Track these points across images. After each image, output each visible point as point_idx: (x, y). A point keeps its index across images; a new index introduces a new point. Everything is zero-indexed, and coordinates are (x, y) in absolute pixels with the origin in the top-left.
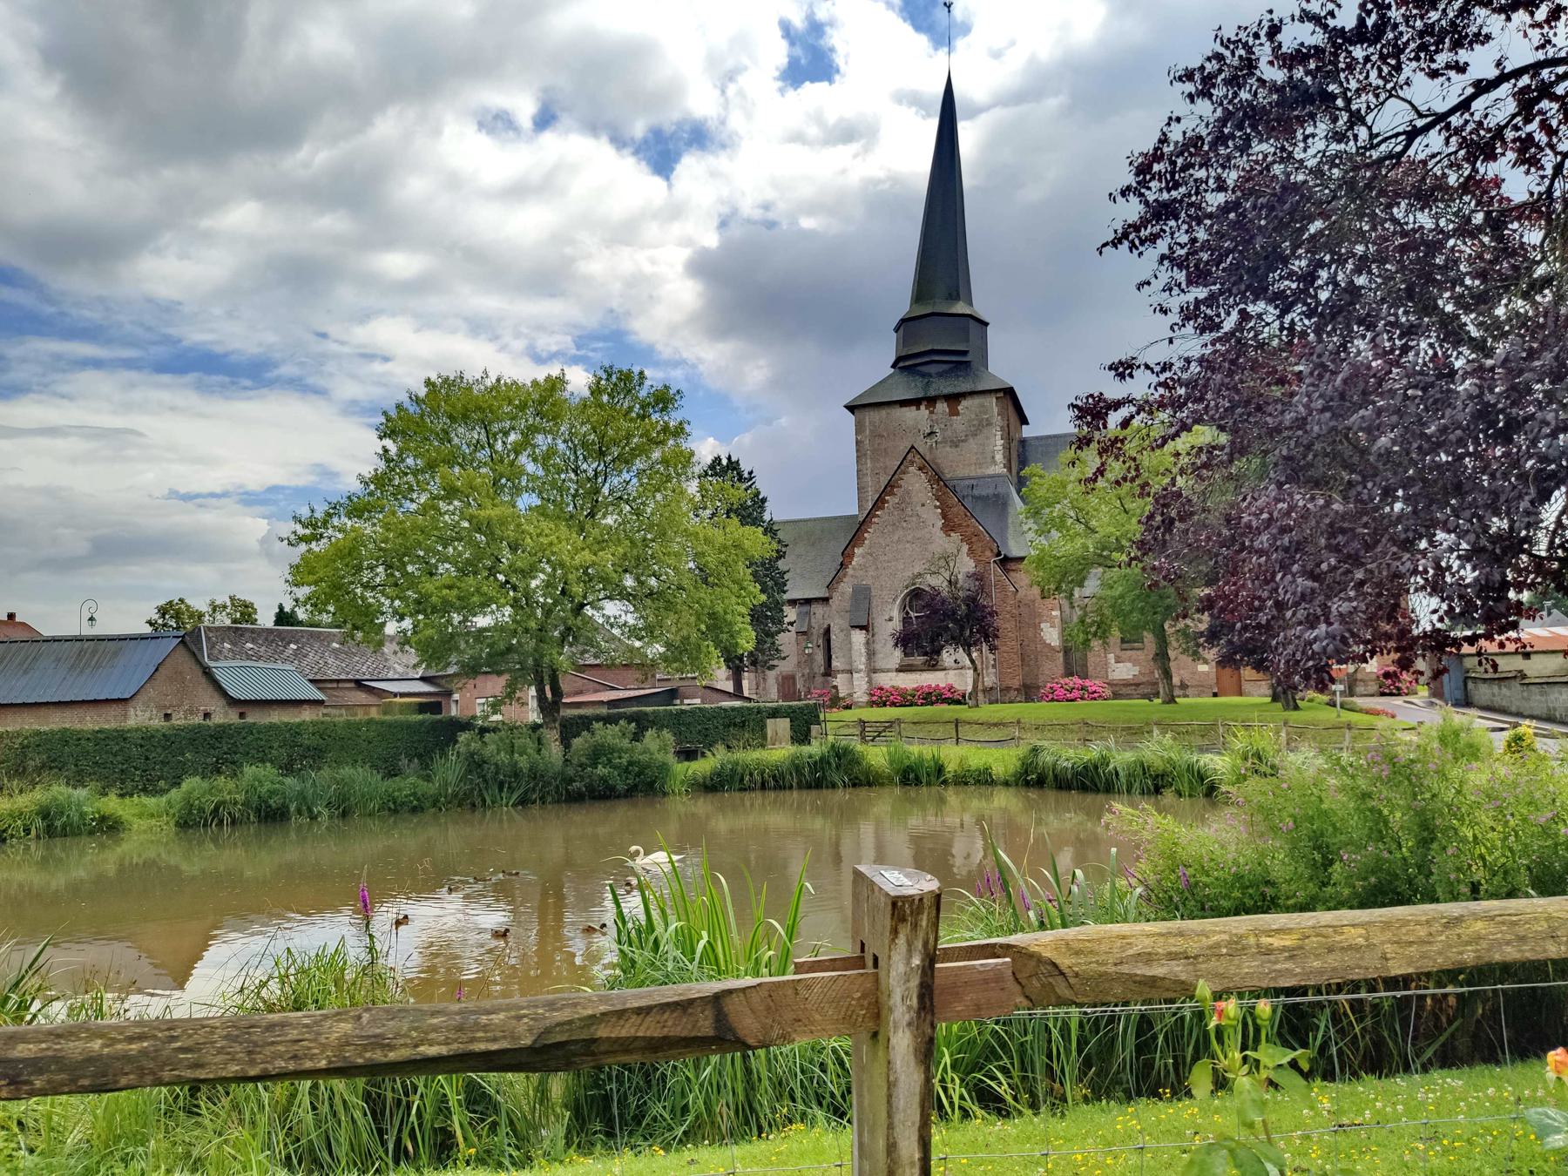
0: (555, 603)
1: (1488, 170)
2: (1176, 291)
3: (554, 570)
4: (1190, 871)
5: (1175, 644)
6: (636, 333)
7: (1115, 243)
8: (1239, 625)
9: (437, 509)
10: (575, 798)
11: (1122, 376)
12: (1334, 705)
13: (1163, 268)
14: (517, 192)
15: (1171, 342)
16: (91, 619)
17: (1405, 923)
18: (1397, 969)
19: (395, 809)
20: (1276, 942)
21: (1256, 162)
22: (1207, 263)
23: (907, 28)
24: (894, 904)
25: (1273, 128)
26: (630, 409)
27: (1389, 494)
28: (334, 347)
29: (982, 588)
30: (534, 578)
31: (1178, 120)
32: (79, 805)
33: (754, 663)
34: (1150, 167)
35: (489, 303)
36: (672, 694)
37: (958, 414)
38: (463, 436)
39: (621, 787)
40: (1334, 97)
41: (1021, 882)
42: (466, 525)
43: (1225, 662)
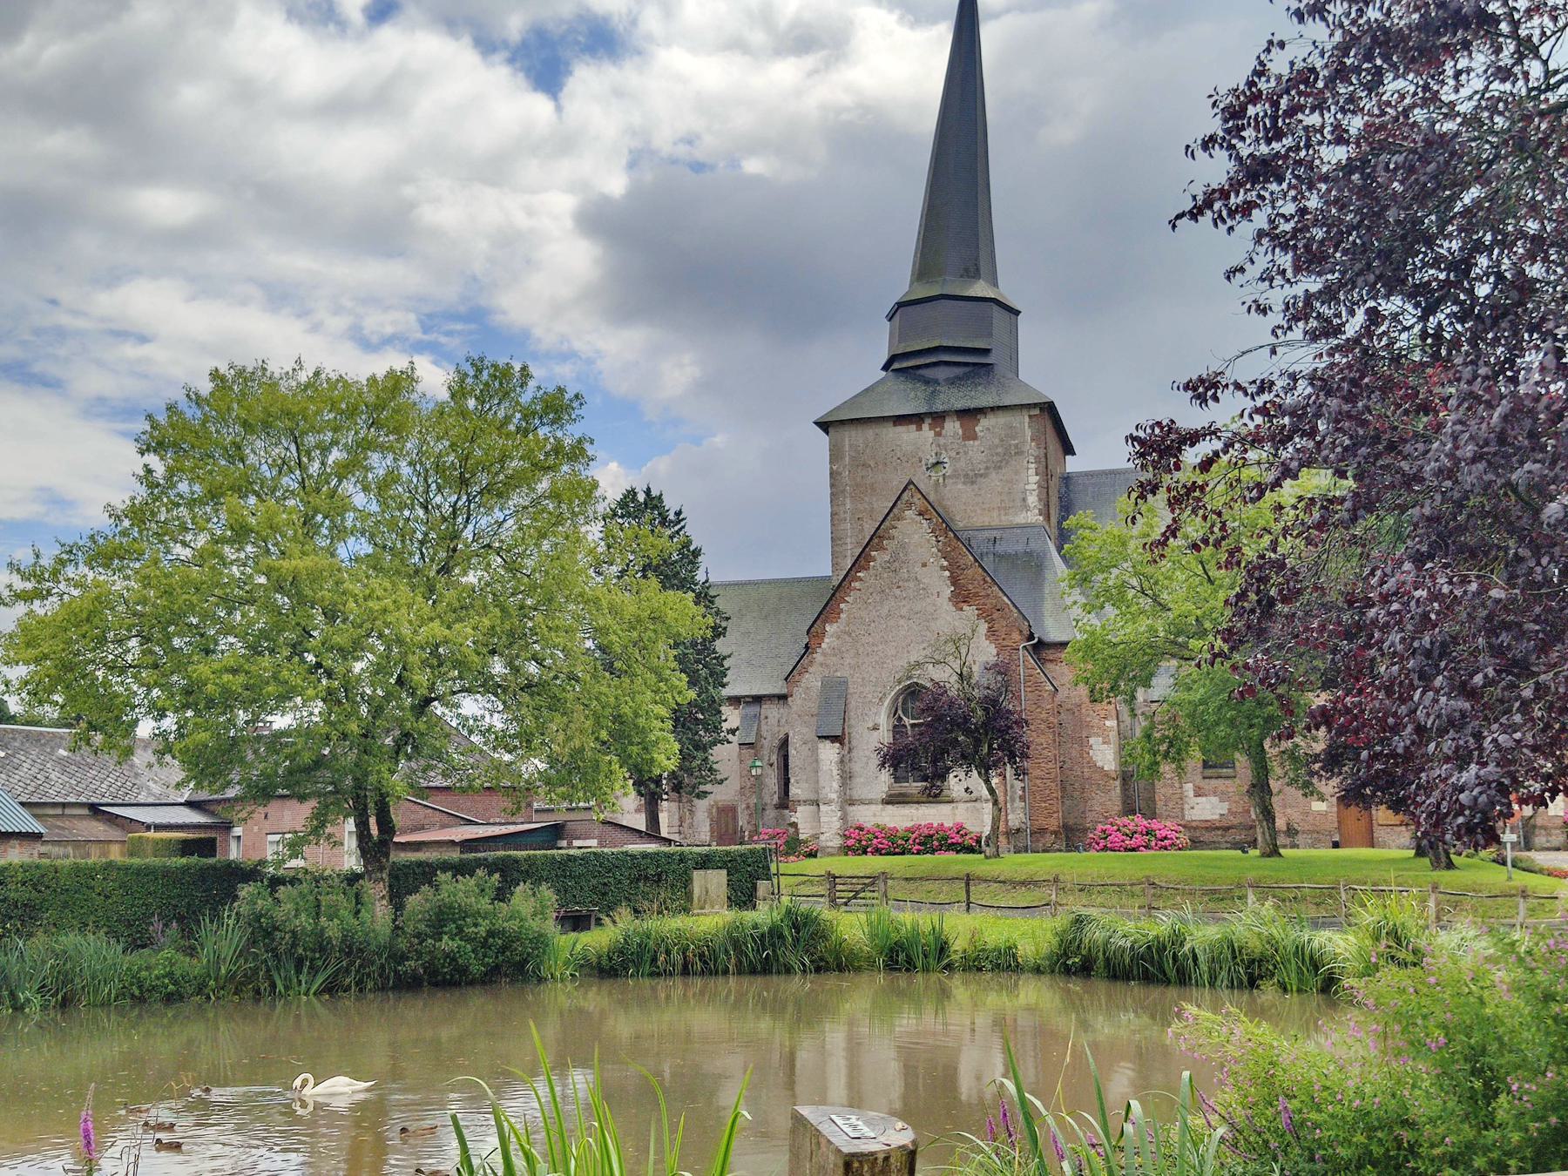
0: (389, 696)
2: (1278, 280)
3: (389, 648)
4: (1295, 1104)
5: (1279, 771)
6: (504, 313)
7: (1195, 214)
8: (1364, 754)
9: (222, 558)
10: (409, 985)
11: (1202, 399)
12: (1504, 863)
13: (1261, 250)
15: (1273, 352)
19: (141, 997)
21: (1388, 104)
22: (1322, 242)
24: (847, 1166)
25: (1413, 60)
28: (65, 320)
29: (1006, 685)
30: (357, 659)
31: (1282, 45)
33: (677, 788)
34: (1244, 109)
36: (556, 832)
37: (975, 438)
38: (261, 455)
39: (476, 968)
40: (1494, 20)
41: (1050, 1120)
42: (262, 580)
43: (1351, 797)
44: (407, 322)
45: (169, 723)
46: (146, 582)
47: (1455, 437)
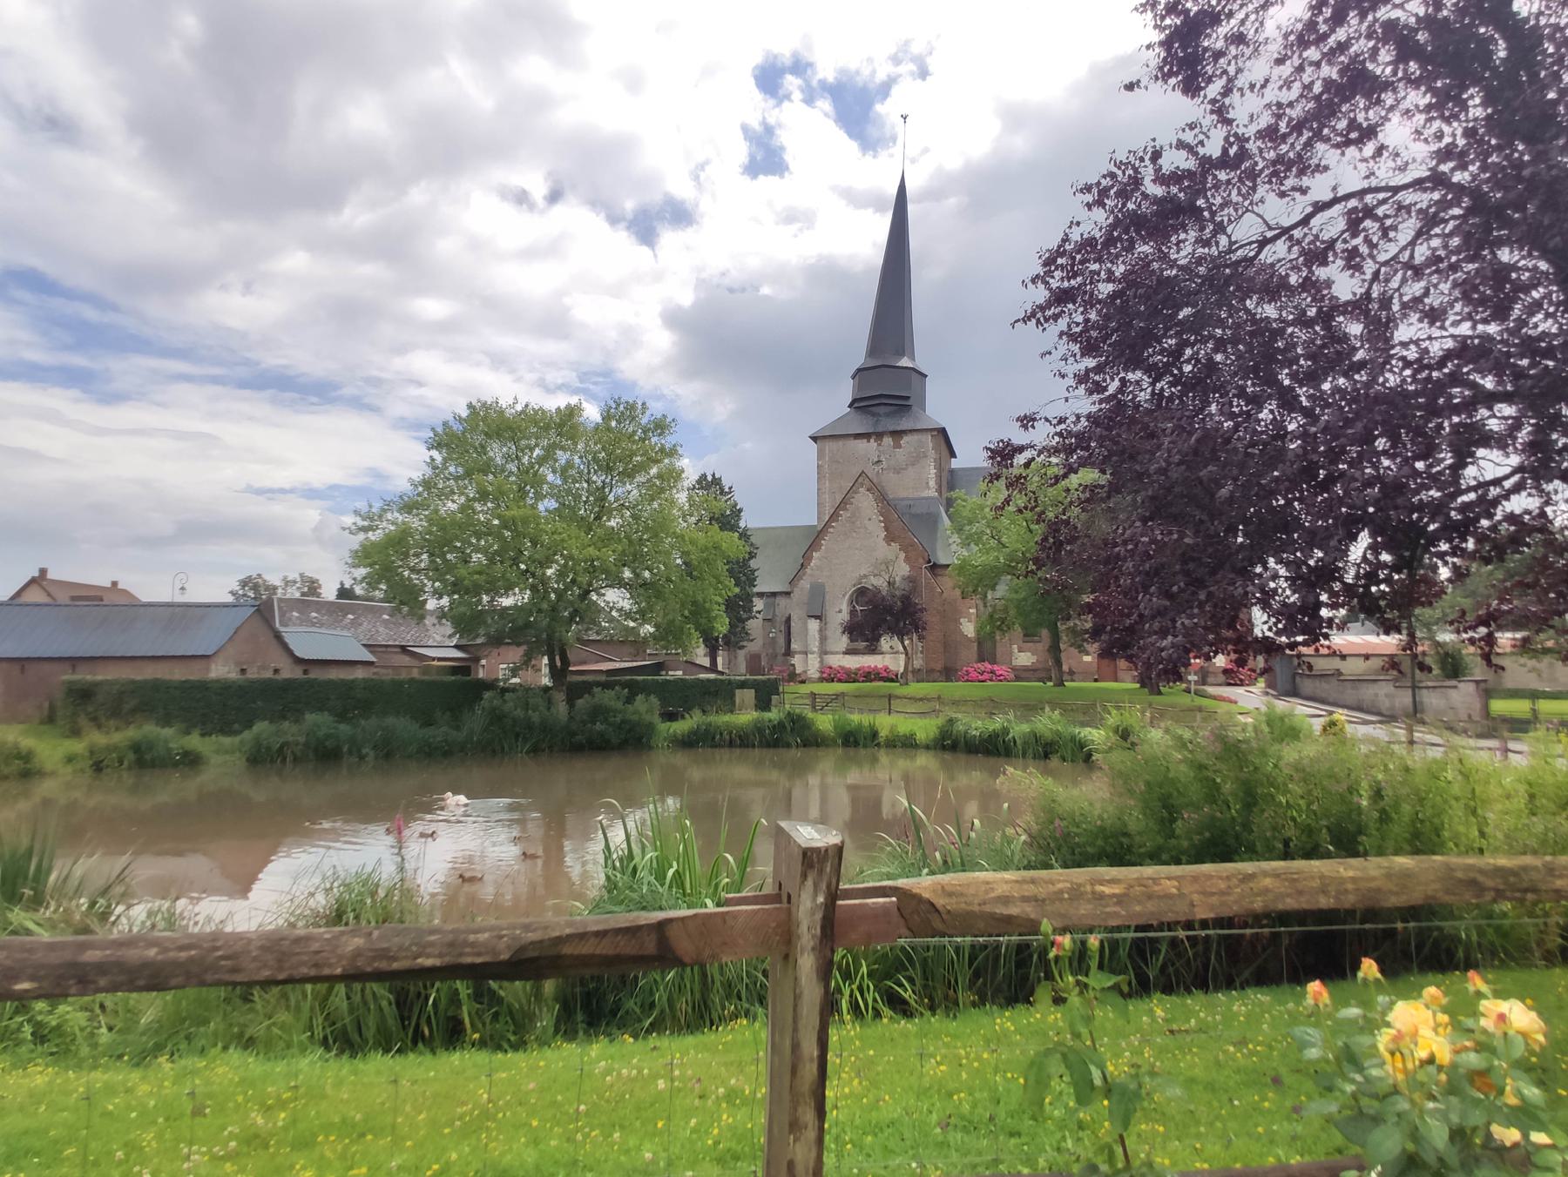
0: (566, 590)
1: (1321, 273)
11: (1025, 427)
14: (528, 254)
16: (183, 588)
17: (1210, 877)
18: (1202, 914)
20: (1107, 890)
23: (840, 135)
26: (634, 432)
27: (1233, 531)
31: (1078, 224)
32: (166, 741)
35: (507, 342)
36: (659, 667)
38: (496, 452)
39: (615, 741)
40: (1201, 210)
43: (1106, 654)
44: (570, 377)
45: (445, 601)
46: (429, 520)
47: (1169, 451)
